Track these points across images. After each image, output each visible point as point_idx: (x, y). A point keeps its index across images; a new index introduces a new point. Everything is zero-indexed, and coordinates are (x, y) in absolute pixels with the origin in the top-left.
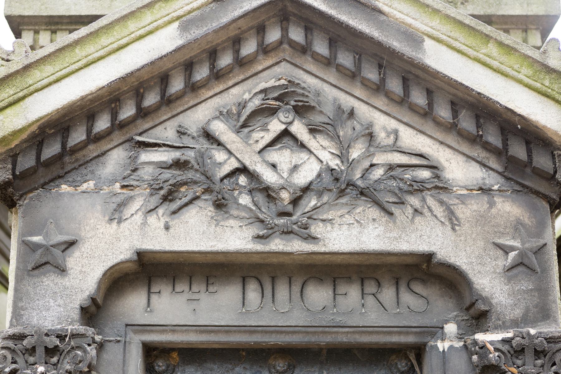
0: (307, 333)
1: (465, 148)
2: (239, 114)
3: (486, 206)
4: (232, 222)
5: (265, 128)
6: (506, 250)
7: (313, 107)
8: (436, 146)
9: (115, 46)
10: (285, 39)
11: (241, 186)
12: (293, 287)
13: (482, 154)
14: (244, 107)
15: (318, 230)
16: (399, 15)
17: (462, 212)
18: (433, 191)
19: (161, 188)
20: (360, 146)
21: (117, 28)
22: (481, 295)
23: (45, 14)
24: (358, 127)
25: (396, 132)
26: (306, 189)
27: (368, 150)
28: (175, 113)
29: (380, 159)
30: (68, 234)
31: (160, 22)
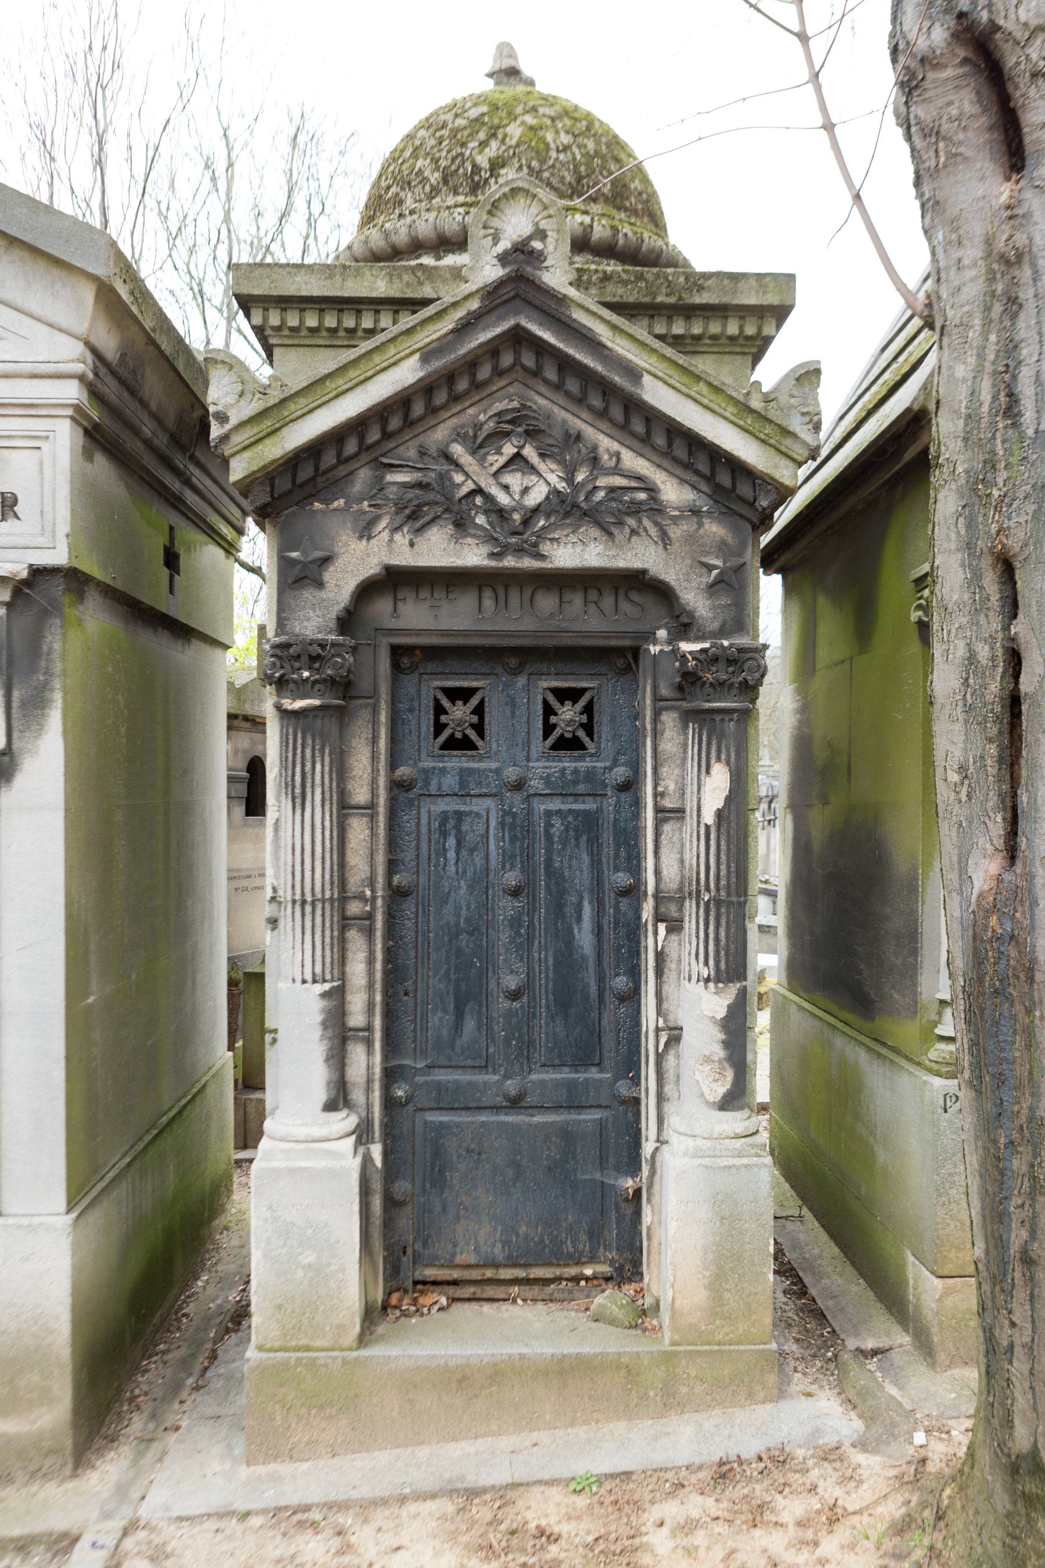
0: (536, 637)
1: (679, 471)
2: (475, 437)
3: (695, 527)
4: (469, 540)
5: (499, 452)
6: (710, 568)
7: (543, 431)
8: (653, 469)
9: (362, 378)
10: (517, 362)
11: (478, 506)
12: (524, 595)
13: (694, 479)
14: (480, 429)
15: (546, 548)
16: (621, 351)
17: (675, 532)
18: (649, 512)
19: (406, 507)
20: (585, 469)
21: (363, 361)
22: (685, 609)
23: (275, 293)
24: (584, 450)
25: (618, 455)
26: (536, 510)
27: (591, 474)
28: (416, 433)
29: (602, 482)
30: (322, 550)
31: (402, 354)
